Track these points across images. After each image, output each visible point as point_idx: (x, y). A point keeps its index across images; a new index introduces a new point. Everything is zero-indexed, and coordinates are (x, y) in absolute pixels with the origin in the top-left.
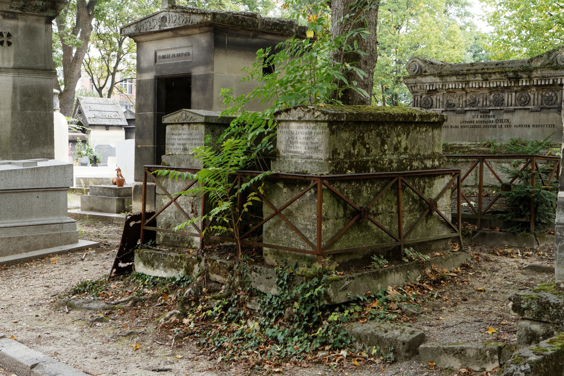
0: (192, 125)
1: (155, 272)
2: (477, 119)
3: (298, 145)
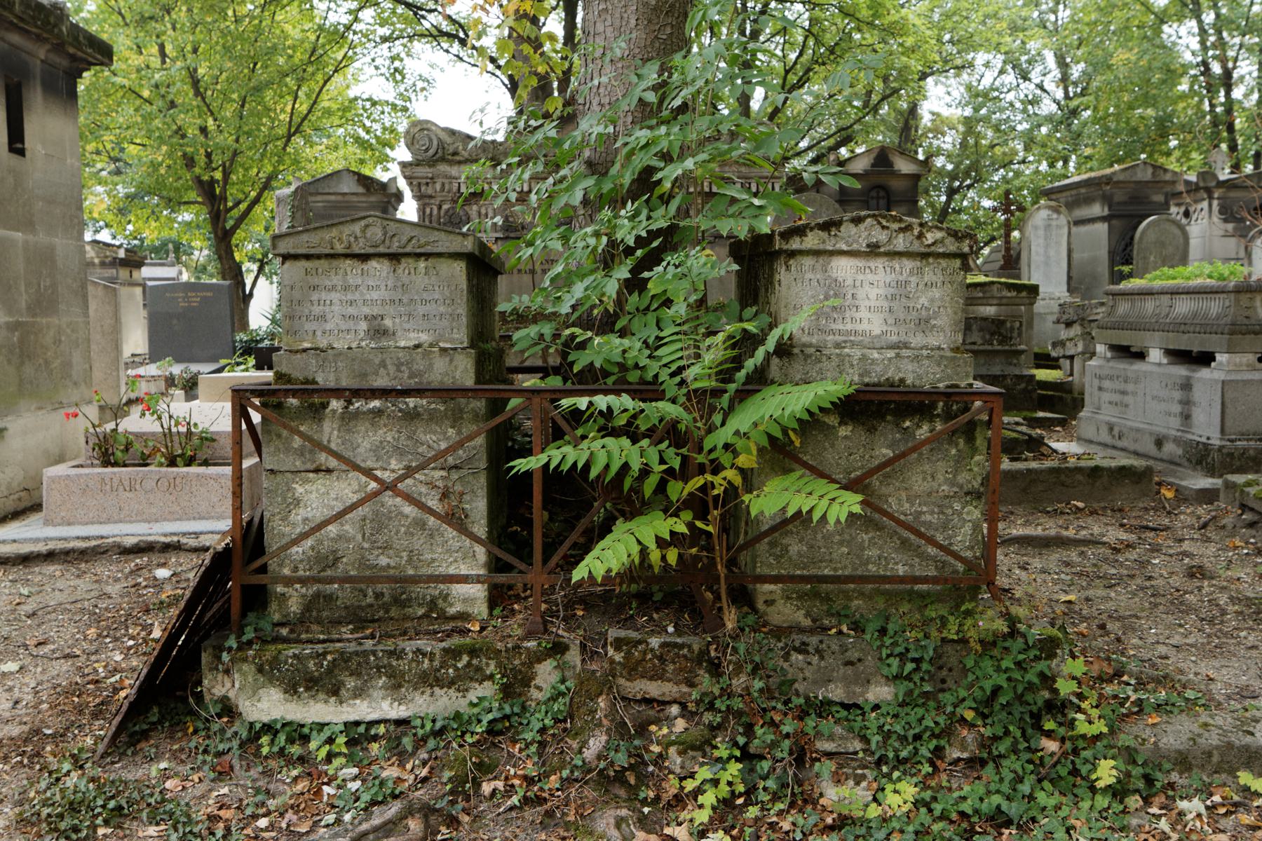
1: (345, 708)
3: (858, 315)
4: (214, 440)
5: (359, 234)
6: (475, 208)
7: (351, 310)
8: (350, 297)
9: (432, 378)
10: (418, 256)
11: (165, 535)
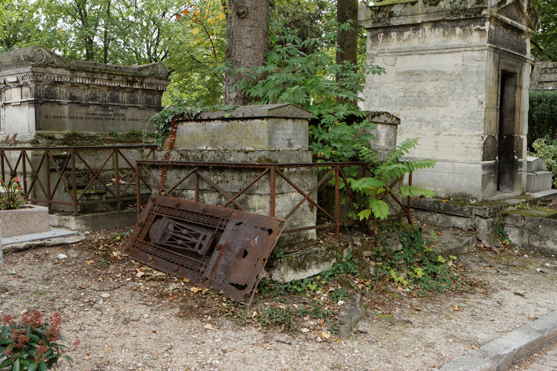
0: (296, 120)
2: (99, 112)
6: (58, 88)
11: (30, 241)
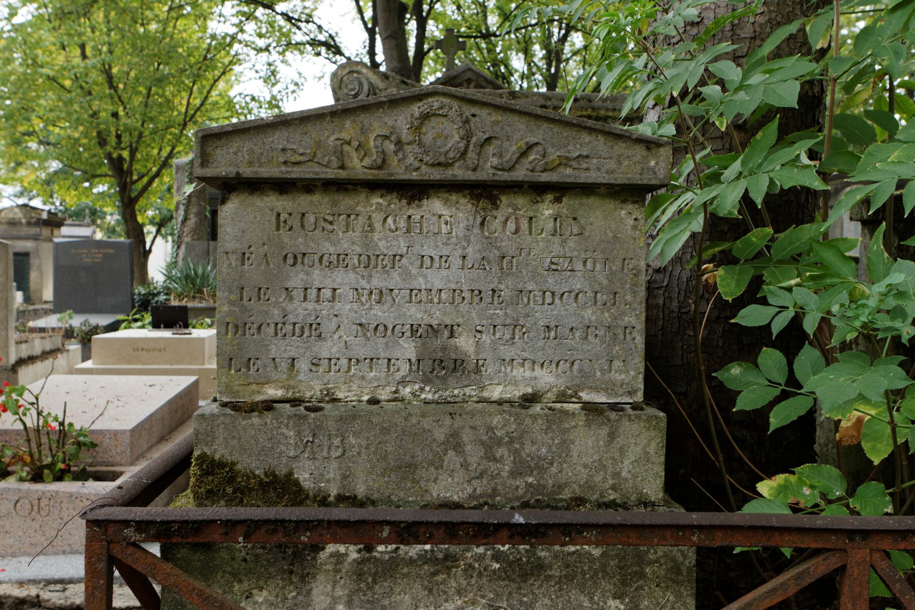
4: (94, 445)
5: (406, 136)
7: (380, 313)
8: (378, 281)
9: (568, 473)
10: (538, 190)
11: (21, 583)
